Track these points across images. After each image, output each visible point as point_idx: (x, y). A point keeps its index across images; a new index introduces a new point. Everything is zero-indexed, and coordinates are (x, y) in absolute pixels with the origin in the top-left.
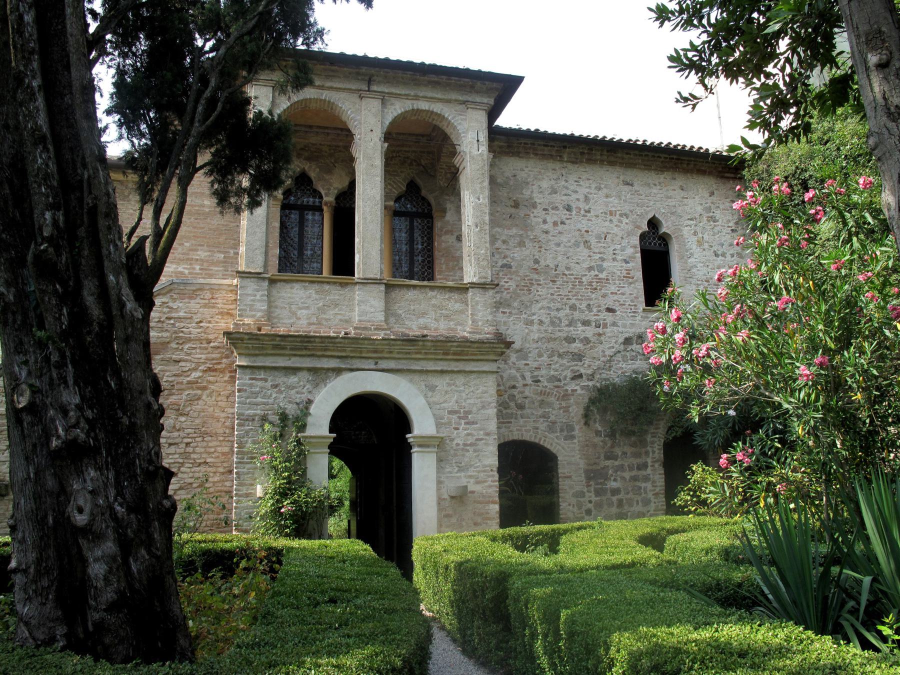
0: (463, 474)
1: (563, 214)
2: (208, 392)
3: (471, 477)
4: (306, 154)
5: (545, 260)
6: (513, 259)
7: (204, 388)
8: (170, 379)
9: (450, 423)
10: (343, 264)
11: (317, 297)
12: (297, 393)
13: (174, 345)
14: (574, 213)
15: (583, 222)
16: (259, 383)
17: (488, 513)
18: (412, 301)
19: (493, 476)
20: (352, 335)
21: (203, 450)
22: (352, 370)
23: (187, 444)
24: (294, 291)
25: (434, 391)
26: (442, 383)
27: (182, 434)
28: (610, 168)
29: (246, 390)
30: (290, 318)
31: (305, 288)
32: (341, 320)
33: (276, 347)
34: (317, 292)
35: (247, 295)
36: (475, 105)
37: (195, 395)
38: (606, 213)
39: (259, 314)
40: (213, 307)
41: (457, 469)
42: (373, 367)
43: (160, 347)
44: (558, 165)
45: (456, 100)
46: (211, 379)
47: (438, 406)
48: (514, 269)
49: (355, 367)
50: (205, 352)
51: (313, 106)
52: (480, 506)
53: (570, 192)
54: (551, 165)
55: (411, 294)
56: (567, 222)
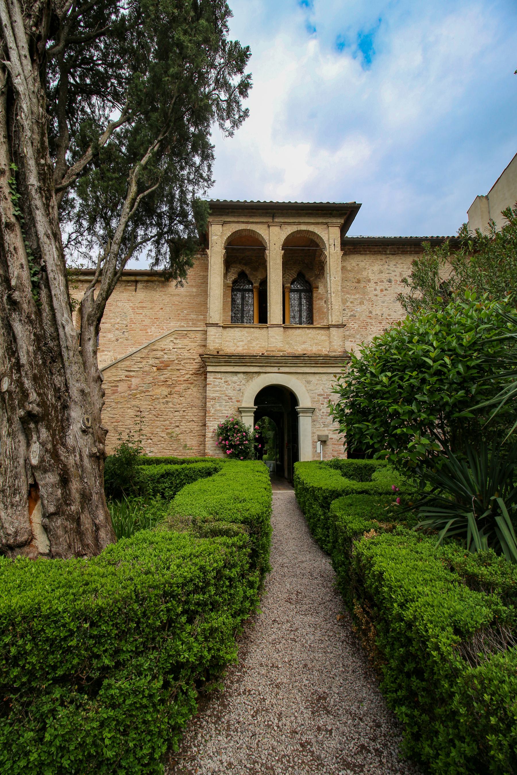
0: (326, 429)
1: (386, 284)
3: (330, 430)
4: (244, 262)
5: (376, 311)
6: (357, 311)
9: (318, 401)
10: (263, 318)
14: (393, 283)
20: (266, 354)
22: (266, 373)
26: (314, 379)
31: (241, 331)
34: (247, 332)
44: (383, 257)
48: (357, 317)
51: (244, 234)
52: (336, 446)
53: (391, 272)
54: (379, 257)
56: (389, 289)
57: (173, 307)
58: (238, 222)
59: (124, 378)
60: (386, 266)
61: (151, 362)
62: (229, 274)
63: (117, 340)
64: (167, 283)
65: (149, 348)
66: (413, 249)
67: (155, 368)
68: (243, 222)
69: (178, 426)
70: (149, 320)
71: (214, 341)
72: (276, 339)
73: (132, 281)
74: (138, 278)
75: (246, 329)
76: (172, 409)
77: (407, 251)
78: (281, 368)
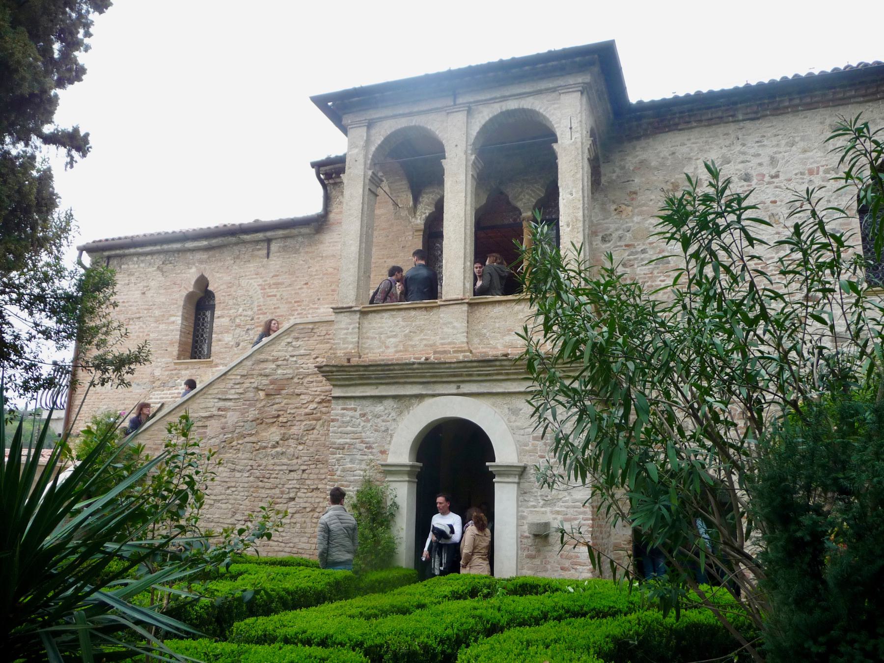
0: (548, 509)
2: (321, 422)
3: (558, 513)
7: (318, 420)
8: (292, 411)
11: (404, 324)
12: (383, 421)
13: (296, 380)
15: (768, 191)
16: (350, 413)
17: (577, 557)
18: (497, 318)
19: (585, 513)
21: (315, 476)
22: (434, 396)
23: (304, 471)
24: (384, 320)
25: (517, 415)
27: (299, 461)
28: (809, 113)
29: (338, 420)
30: (380, 347)
31: (393, 316)
32: (426, 345)
33: (362, 377)
34: (404, 319)
35: (341, 329)
36: (567, 89)
37: (311, 425)
38: (802, 174)
39: (351, 346)
40: (328, 343)
41: (542, 502)
42: (455, 391)
43: (285, 382)
44: (732, 127)
46: (324, 409)
47: (522, 432)
49: (437, 392)
50: (320, 384)
53: (748, 158)
54: (721, 129)
55: (498, 310)
57: (325, 279)
58: (394, 117)
59: (216, 413)
60: (738, 148)
61: (256, 382)
62: (420, 207)
63: (238, 345)
64: (317, 237)
65: (254, 359)
66: (797, 101)
67: (262, 394)
69: (293, 499)
70: (287, 306)
71: (345, 340)
72: (454, 328)
73: (262, 241)
74: (269, 234)
75: (402, 313)
76: (285, 467)
77: (787, 107)
78: (462, 386)
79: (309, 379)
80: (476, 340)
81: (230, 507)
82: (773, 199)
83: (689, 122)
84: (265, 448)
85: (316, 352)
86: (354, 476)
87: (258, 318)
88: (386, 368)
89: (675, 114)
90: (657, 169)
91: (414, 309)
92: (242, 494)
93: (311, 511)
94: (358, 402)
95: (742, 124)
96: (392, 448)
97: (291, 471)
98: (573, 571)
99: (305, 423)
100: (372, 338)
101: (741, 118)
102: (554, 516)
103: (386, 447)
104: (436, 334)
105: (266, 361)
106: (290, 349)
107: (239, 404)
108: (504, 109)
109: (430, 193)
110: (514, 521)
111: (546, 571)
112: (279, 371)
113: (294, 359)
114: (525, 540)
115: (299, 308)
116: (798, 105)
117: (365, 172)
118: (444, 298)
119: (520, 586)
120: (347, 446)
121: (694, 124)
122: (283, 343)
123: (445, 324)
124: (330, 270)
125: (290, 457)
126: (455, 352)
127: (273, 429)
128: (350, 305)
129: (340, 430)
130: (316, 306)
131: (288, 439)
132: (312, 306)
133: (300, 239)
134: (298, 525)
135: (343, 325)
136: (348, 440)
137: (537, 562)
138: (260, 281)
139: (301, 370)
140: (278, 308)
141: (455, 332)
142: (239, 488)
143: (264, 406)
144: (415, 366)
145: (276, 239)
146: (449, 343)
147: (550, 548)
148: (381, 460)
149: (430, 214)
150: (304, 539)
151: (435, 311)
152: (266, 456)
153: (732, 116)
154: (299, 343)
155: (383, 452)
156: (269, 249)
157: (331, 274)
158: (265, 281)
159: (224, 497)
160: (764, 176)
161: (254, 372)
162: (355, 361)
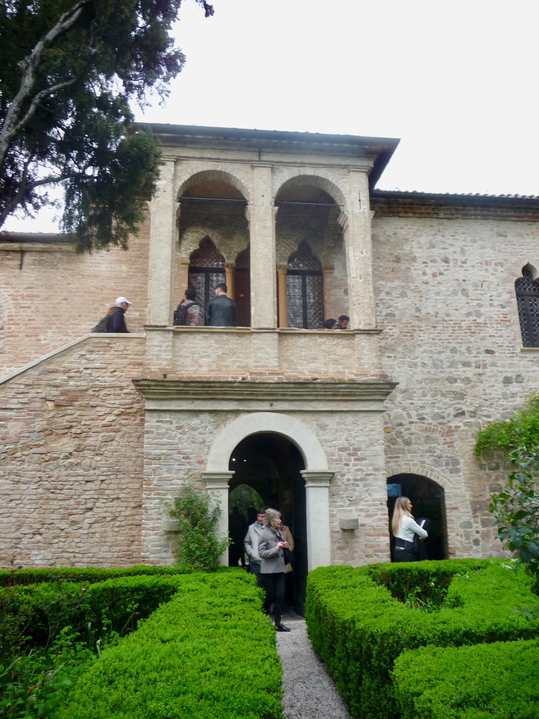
0: (353, 508)
2: (120, 433)
3: (361, 510)
7: (118, 431)
8: (87, 423)
11: (217, 346)
12: (200, 434)
13: (90, 392)
16: (166, 426)
19: (382, 509)
21: (116, 486)
22: (249, 412)
23: (102, 481)
27: (97, 472)
28: (484, 222)
29: (152, 432)
32: (238, 367)
33: (179, 393)
34: (217, 342)
35: (155, 346)
37: (110, 436)
38: (481, 263)
39: (165, 363)
40: (127, 358)
41: (348, 502)
43: (79, 394)
44: (435, 222)
45: (339, 165)
46: (124, 422)
49: (252, 408)
50: (119, 397)
53: (447, 246)
55: (303, 341)
58: (202, 159)
62: (184, 243)
65: (41, 368)
67: (50, 405)
68: (210, 159)
69: (91, 509)
72: (266, 353)
74: (25, 246)
75: (215, 336)
77: (471, 215)
78: (275, 404)
79: (105, 392)
80: (285, 365)
81: (14, 520)
82: (464, 278)
83: (407, 212)
84: (56, 459)
85: (113, 366)
86: (172, 484)
87: (10, 328)
88: (207, 385)
89: (400, 204)
90: (383, 243)
91: (227, 333)
92: (30, 506)
93: (112, 520)
94: (174, 415)
95: (442, 221)
96: (210, 458)
97: (87, 482)
98: (375, 557)
99: (102, 434)
100: (185, 357)
101: (442, 216)
102: (359, 513)
103: (204, 457)
104: (248, 357)
105: (56, 372)
106: (84, 361)
107: (23, 414)
108: (302, 173)
109: (194, 232)
110: (327, 519)
111: (353, 559)
112: (72, 383)
113: (89, 371)
114: (335, 535)
115: (58, 322)
116: (478, 215)
117: (174, 204)
118: (253, 326)
119: (397, 571)
120: (163, 457)
121: (411, 215)
122: (76, 355)
123: (258, 349)
124: (93, 289)
125: (87, 468)
126: (270, 374)
127: (65, 440)
128: (163, 324)
129: (155, 441)
130: (77, 322)
131: (83, 450)
132: (71, 321)
133: (59, 255)
134: (98, 535)
135: (155, 342)
136: (164, 451)
137: (346, 552)
138: (12, 291)
139: (97, 383)
140: (33, 320)
141: (268, 356)
142: (25, 501)
143: (53, 417)
144: (236, 385)
145: (30, 251)
146: (263, 366)
147: (357, 539)
148: (199, 469)
149: (195, 251)
150: (105, 548)
151: (247, 337)
152: (58, 466)
153: (437, 214)
154: (93, 356)
155: (201, 462)
156: (22, 260)
157: (93, 293)
158: (17, 292)
159: (6, 510)
160: (457, 260)
161: (41, 382)
162: (171, 377)
